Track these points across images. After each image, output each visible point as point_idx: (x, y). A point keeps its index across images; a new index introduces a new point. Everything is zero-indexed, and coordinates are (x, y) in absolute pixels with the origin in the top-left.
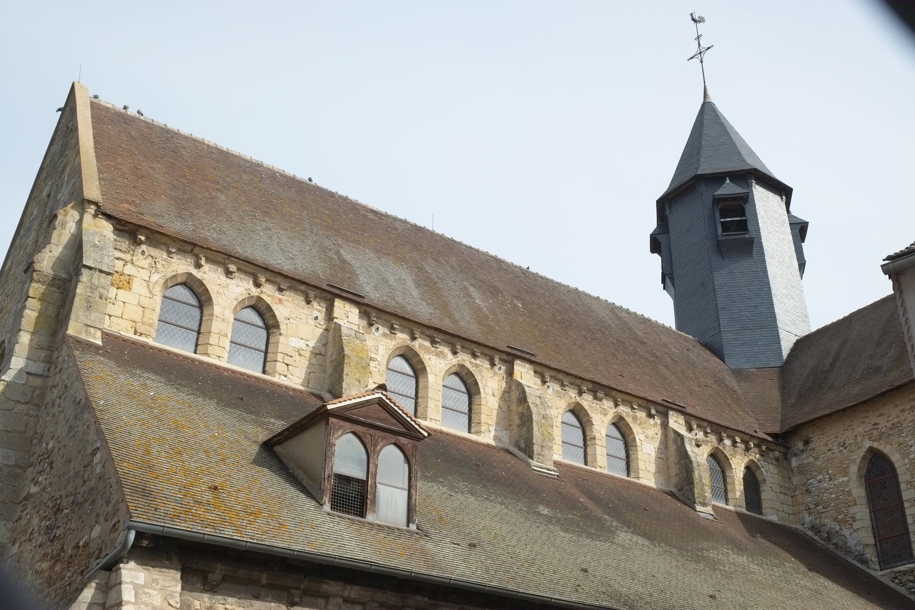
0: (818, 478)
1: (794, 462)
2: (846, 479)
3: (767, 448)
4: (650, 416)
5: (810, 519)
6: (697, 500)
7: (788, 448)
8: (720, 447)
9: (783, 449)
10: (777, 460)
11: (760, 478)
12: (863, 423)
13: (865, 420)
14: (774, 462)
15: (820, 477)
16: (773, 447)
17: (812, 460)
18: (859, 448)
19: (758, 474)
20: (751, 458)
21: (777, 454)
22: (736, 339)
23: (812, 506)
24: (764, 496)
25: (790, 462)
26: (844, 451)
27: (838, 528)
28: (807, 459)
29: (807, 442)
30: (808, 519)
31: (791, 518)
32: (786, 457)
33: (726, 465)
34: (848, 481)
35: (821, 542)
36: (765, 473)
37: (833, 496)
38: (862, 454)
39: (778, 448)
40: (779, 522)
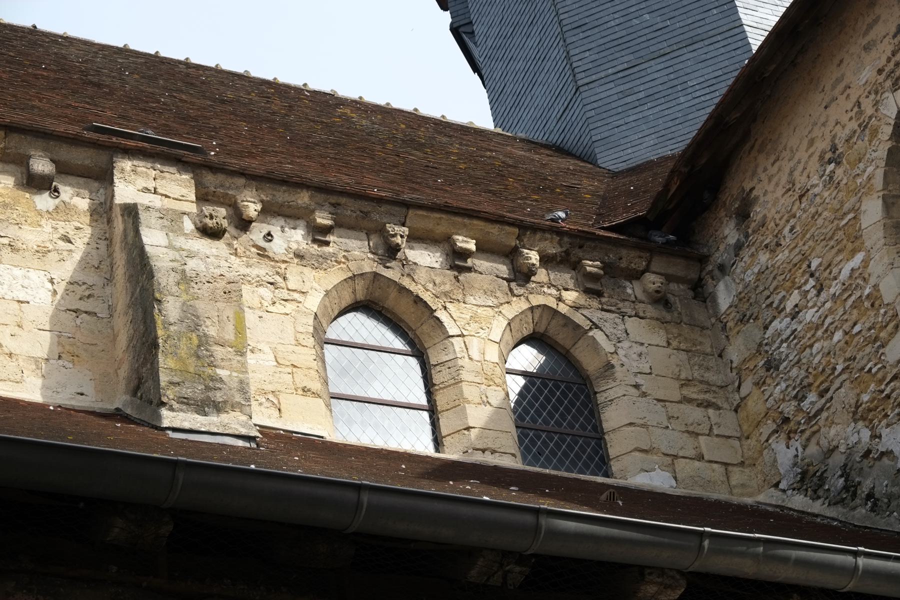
0: (789, 305)
1: (725, 296)
2: (859, 257)
3: (606, 266)
4: (36, 183)
5: (791, 452)
6: (169, 394)
7: (703, 260)
8: (392, 273)
9: (677, 268)
10: (661, 300)
11: (590, 364)
12: (867, 48)
13: (872, 36)
14: (651, 310)
15: (795, 298)
16: (631, 259)
17: (763, 257)
18: (875, 133)
19: (581, 353)
20: (537, 300)
21: (653, 281)
22: (624, 94)
23: (789, 408)
24: (612, 418)
25: (714, 300)
26: (839, 172)
27: (866, 434)
28: (754, 264)
29: (743, 215)
30: (784, 454)
31: (737, 476)
32: (700, 291)
33: (424, 330)
34: (866, 263)
35: (831, 512)
36: (607, 346)
37: (838, 336)
38: (882, 152)
39: (658, 264)
40: (680, 492)
